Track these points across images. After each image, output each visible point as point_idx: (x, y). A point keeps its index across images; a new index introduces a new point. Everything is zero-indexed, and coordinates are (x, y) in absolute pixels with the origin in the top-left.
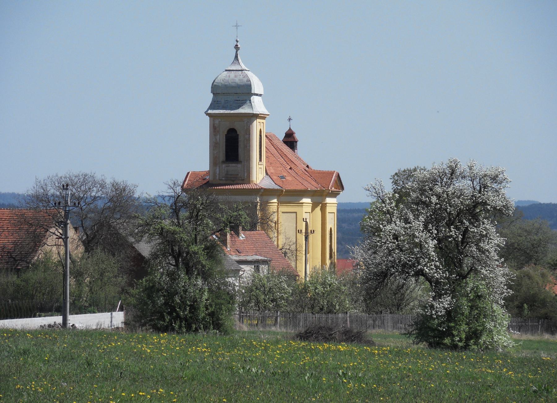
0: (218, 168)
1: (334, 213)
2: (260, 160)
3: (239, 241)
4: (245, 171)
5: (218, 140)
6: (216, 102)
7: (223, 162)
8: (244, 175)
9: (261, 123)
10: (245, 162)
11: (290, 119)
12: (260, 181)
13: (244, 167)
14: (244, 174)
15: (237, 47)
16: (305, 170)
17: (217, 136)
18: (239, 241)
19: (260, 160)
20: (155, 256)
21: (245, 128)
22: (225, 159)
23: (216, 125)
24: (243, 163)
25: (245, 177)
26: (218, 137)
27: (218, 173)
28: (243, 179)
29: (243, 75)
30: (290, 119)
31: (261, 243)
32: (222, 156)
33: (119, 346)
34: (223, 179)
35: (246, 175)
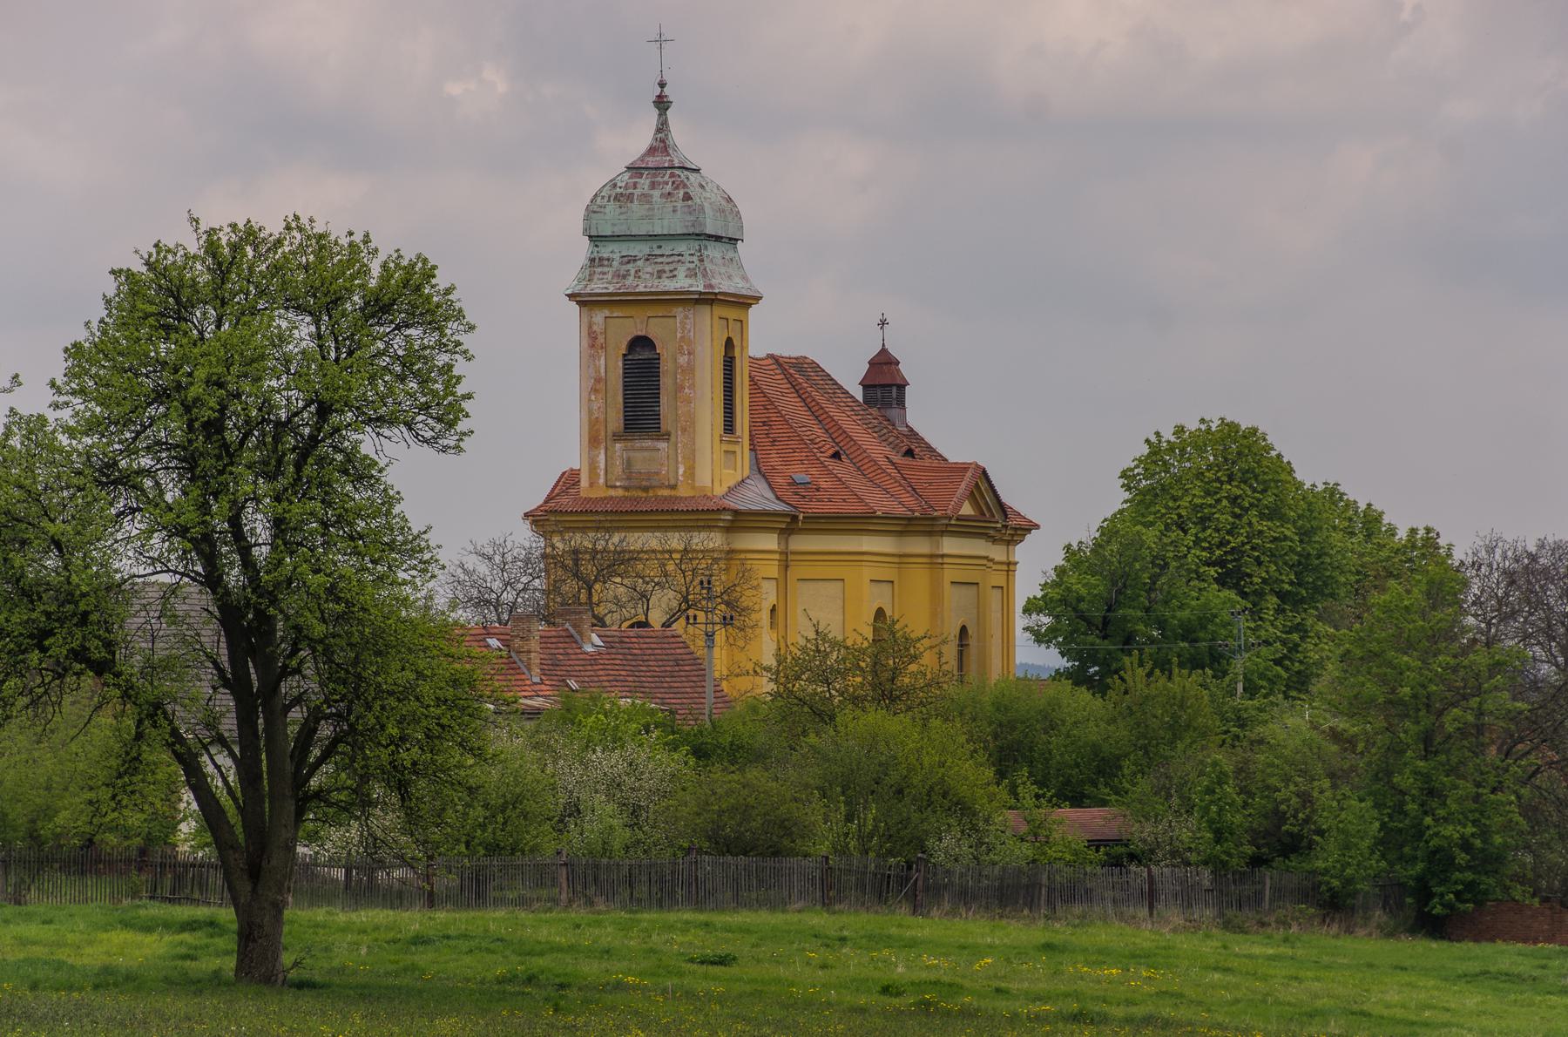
0: (603, 451)
1: (892, 582)
2: (729, 427)
3: (581, 656)
4: (680, 459)
5: (603, 371)
6: (597, 261)
7: (617, 437)
8: (677, 473)
9: (731, 322)
10: (679, 433)
11: (883, 323)
12: (726, 489)
13: (677, 450)
14: (677, 468)
15: (662, 104)
16: (890, 461)
17: (599, 360)
18: (581, 656)
19: (729, 427)
20: (1423, 819)
21: (679, 335)
22: (622, 425)
23: (595, 328)
24: (673, 439)
25: (680, 478)
26: (602, 361)
27: (602, 465)
28: (672, 482)
29: (673, 182)
30: (883, 323)
31: (660, 663)
32: (616, 420)
33: (1134, 980)
34: (618, 484)
35: (681, 471)
